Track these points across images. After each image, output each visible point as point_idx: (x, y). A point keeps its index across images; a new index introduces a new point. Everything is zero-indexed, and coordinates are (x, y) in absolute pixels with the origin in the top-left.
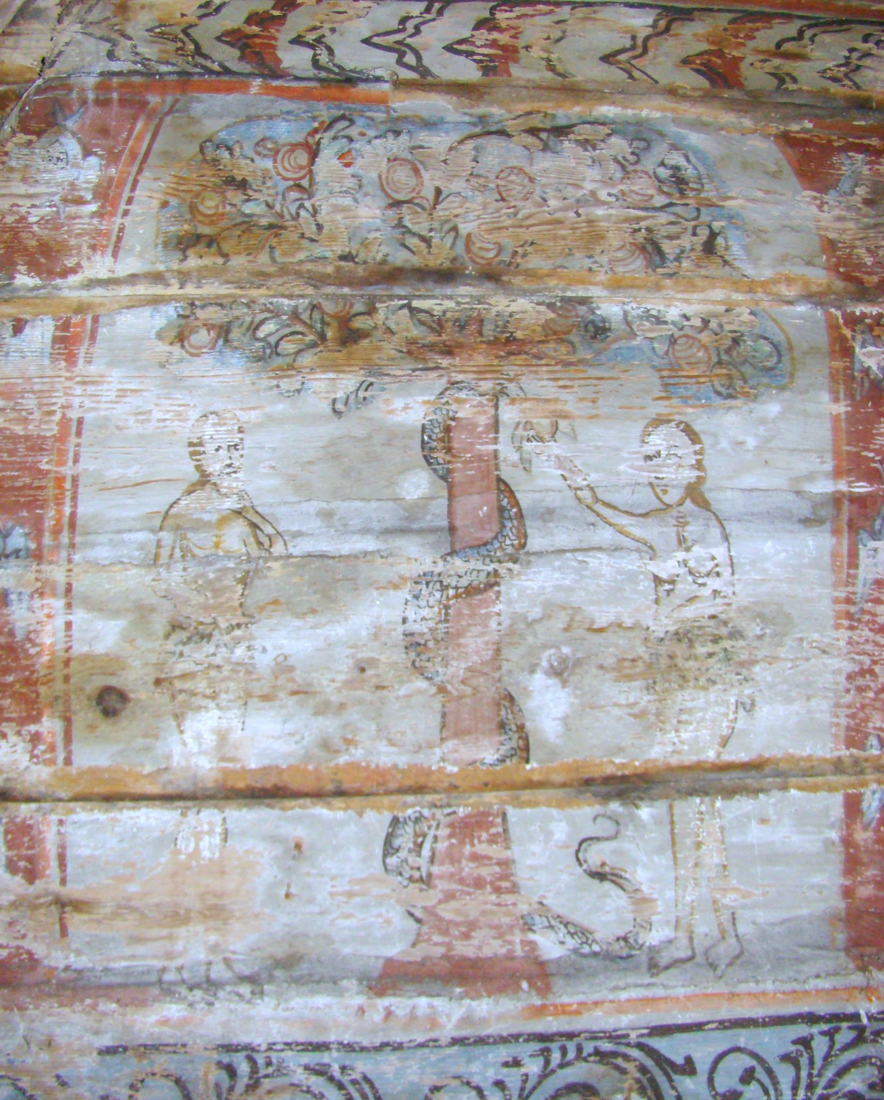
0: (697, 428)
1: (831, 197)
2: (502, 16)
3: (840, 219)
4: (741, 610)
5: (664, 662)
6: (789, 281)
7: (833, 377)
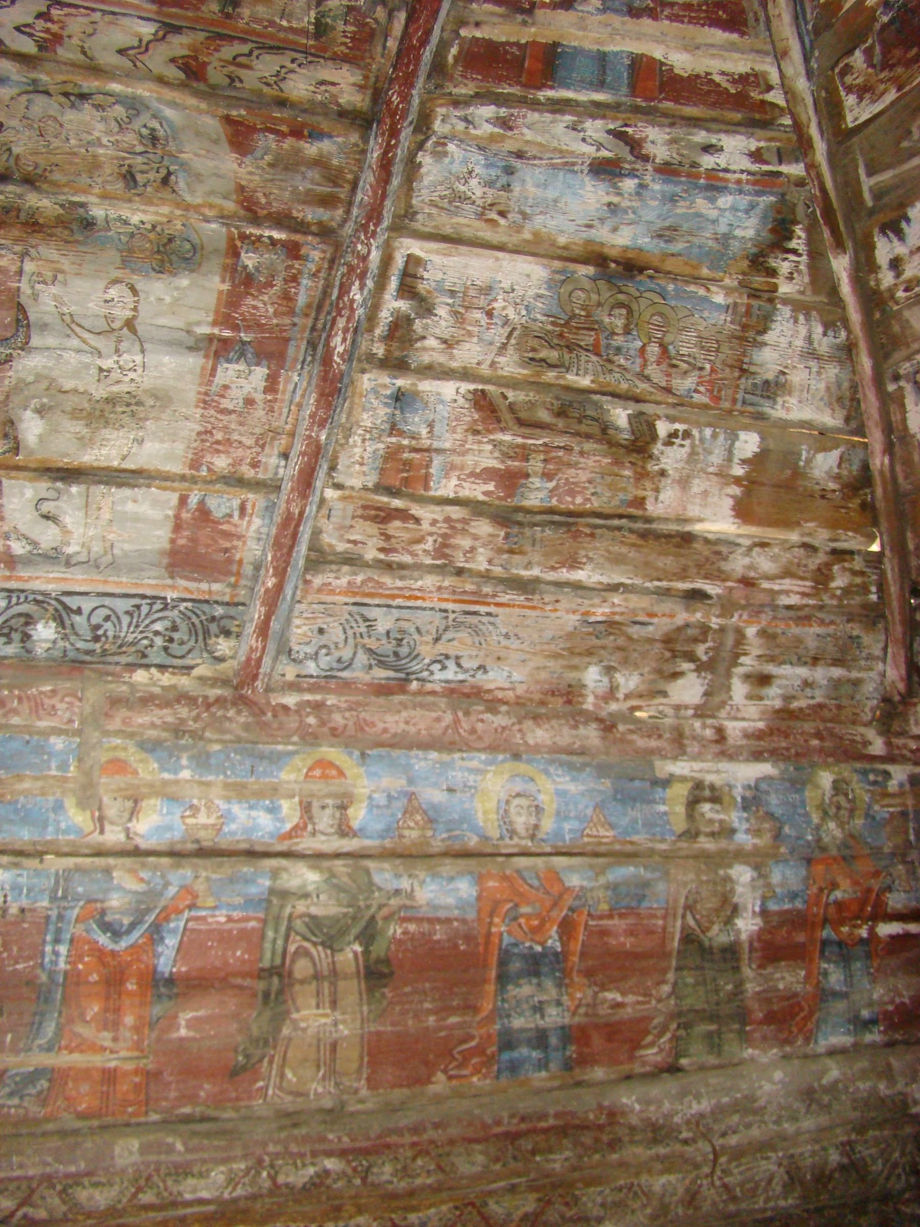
0: (138, 287)
1: (248, 160)
2: (55, 12)
3: (251, 173)
4: (145, 391)
5: (98, 413)
6: (211, 206)
7: (225, 268)
